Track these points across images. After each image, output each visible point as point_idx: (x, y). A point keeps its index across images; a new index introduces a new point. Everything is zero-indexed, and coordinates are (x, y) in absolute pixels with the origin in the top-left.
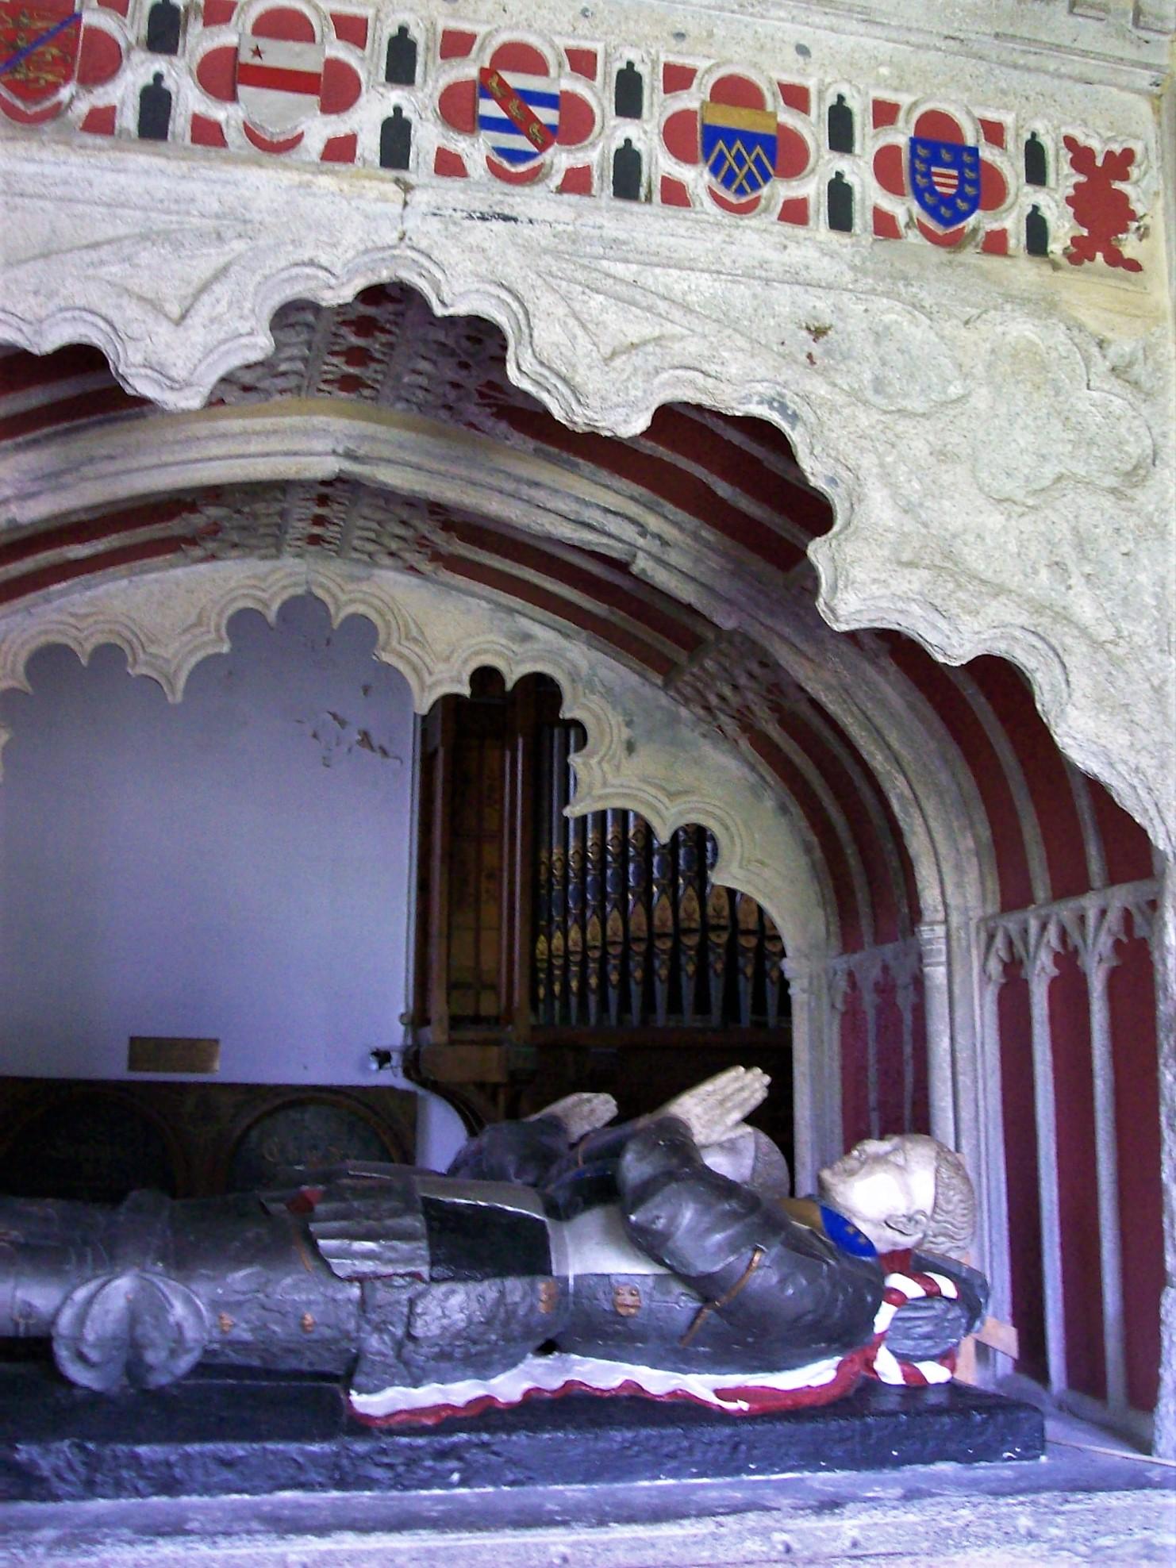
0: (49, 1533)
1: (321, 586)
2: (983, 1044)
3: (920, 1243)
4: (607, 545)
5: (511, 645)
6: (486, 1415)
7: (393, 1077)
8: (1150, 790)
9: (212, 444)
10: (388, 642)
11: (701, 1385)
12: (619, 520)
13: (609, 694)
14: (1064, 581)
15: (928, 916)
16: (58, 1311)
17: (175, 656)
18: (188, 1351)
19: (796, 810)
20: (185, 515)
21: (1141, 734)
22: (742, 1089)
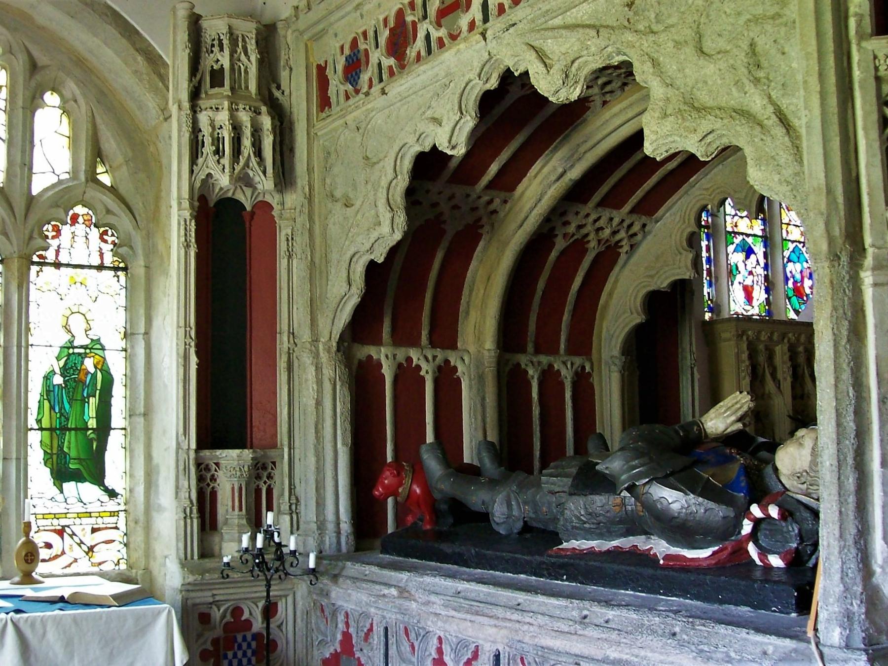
9: (615, 119)
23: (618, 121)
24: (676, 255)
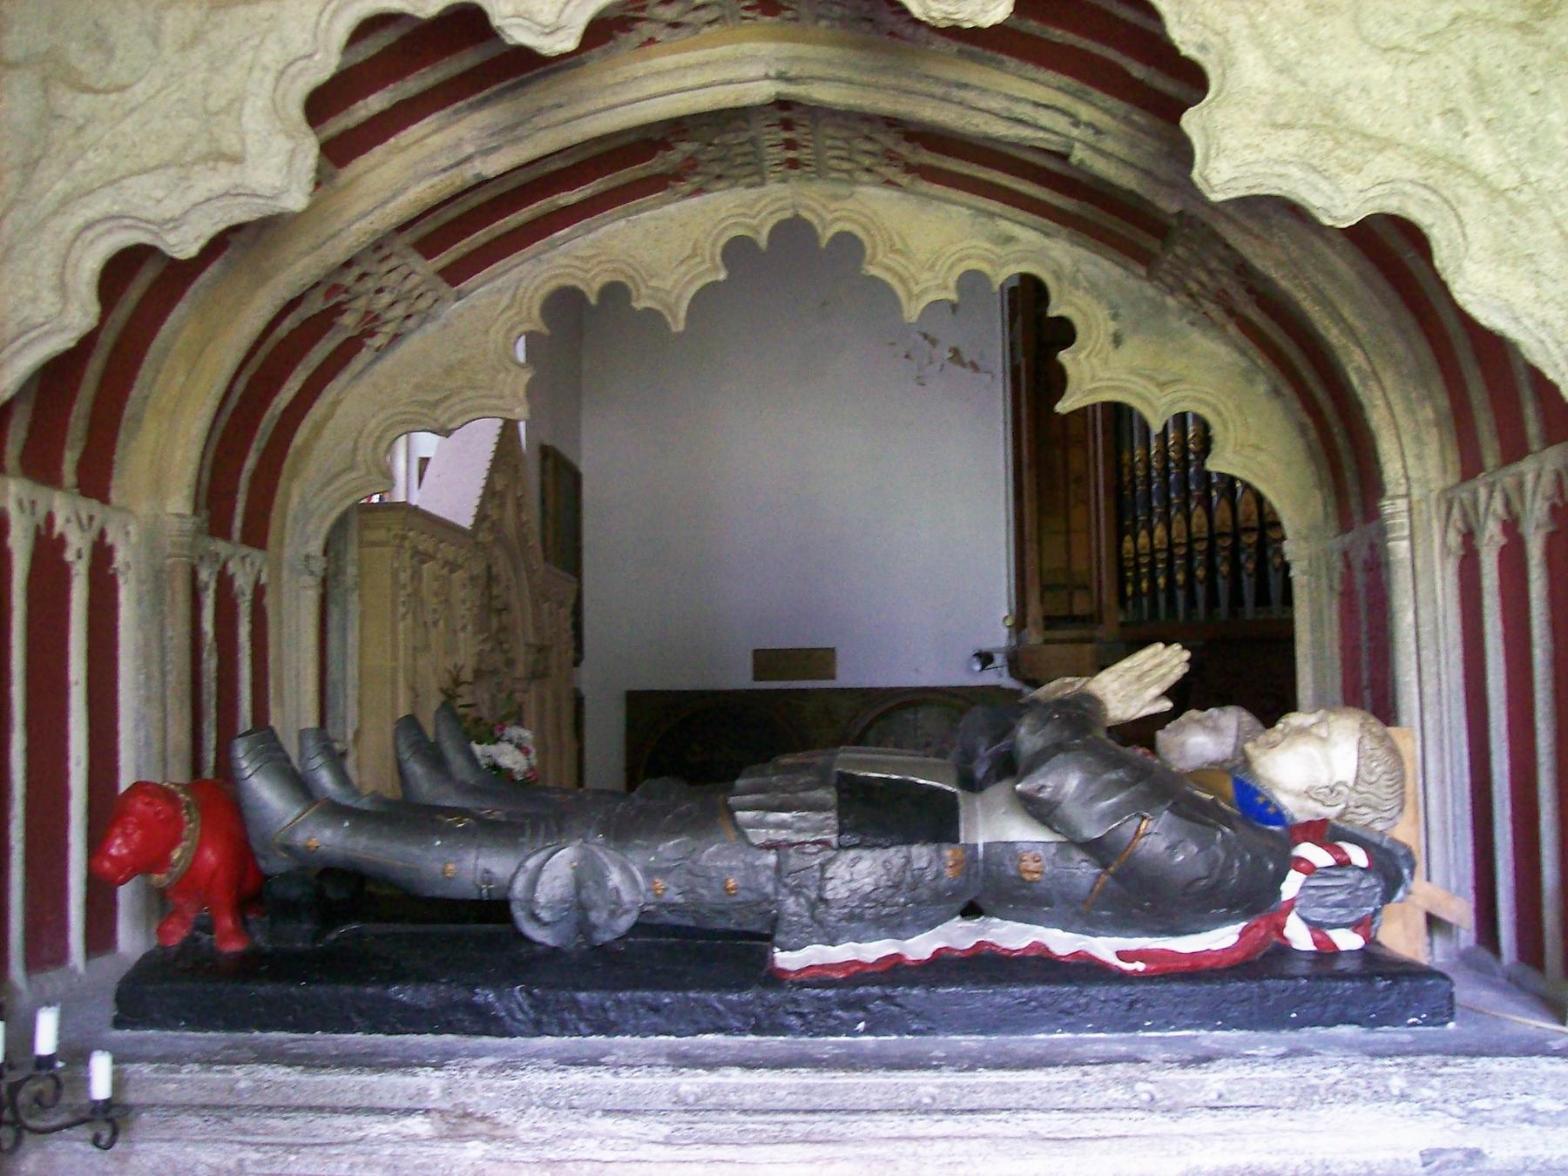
0: (489, 1061)
1: (807, 208)
2: (1445, 617)
3: (1340, 817)
4: (1046, 140)
5: (993, 248)
6: (894, 970)
7: (999, 677)
8: (1559, 344)
10: (874, 255)
11: (1105, 947)
12: (1050, 112)
13: (1093, 289)
14: (1460, 128)
15: (1391, 489)
16: (514, 877)
17: (674, 286)
18: (627, 912)
19: (1287, 391)
20: (660, 153)
21: (1547, 285)
22: (1160, 665)
23: (654, 86)
24: (499, 372)
